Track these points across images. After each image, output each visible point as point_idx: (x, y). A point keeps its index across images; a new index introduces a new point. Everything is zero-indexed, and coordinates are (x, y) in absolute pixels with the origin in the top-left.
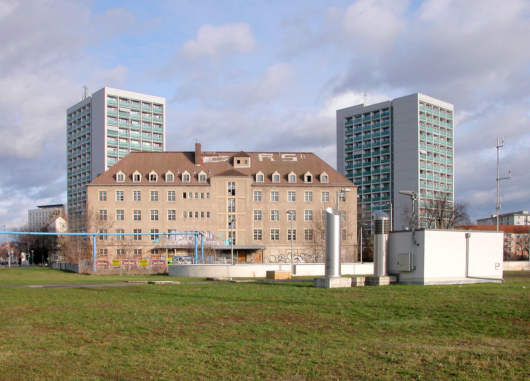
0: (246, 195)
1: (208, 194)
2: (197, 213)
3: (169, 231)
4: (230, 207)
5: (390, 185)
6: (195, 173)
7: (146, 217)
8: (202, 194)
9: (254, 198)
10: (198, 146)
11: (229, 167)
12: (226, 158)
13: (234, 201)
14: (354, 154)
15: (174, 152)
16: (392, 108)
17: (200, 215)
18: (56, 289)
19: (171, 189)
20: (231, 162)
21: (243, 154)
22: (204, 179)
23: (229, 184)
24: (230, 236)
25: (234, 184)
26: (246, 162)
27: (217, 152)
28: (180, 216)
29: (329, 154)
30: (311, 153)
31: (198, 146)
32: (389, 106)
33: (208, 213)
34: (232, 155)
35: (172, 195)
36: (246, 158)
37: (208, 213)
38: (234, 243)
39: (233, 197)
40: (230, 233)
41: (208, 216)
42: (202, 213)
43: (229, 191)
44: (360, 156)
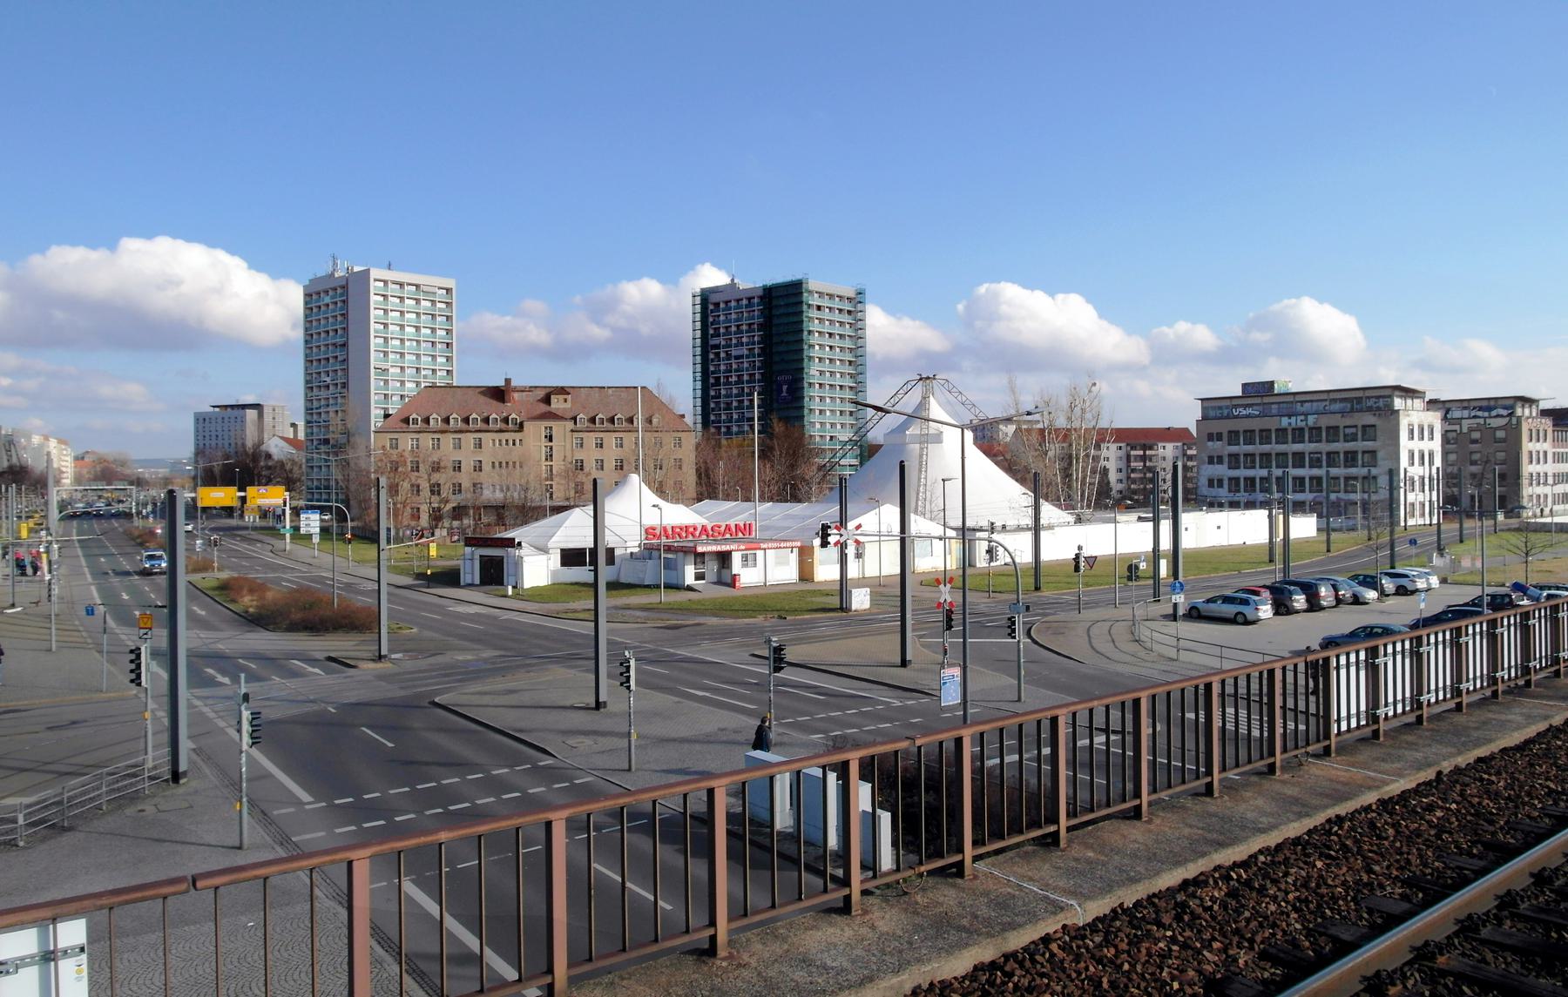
10: (508, 381)
21: (562, 391)
31: (508, 381)
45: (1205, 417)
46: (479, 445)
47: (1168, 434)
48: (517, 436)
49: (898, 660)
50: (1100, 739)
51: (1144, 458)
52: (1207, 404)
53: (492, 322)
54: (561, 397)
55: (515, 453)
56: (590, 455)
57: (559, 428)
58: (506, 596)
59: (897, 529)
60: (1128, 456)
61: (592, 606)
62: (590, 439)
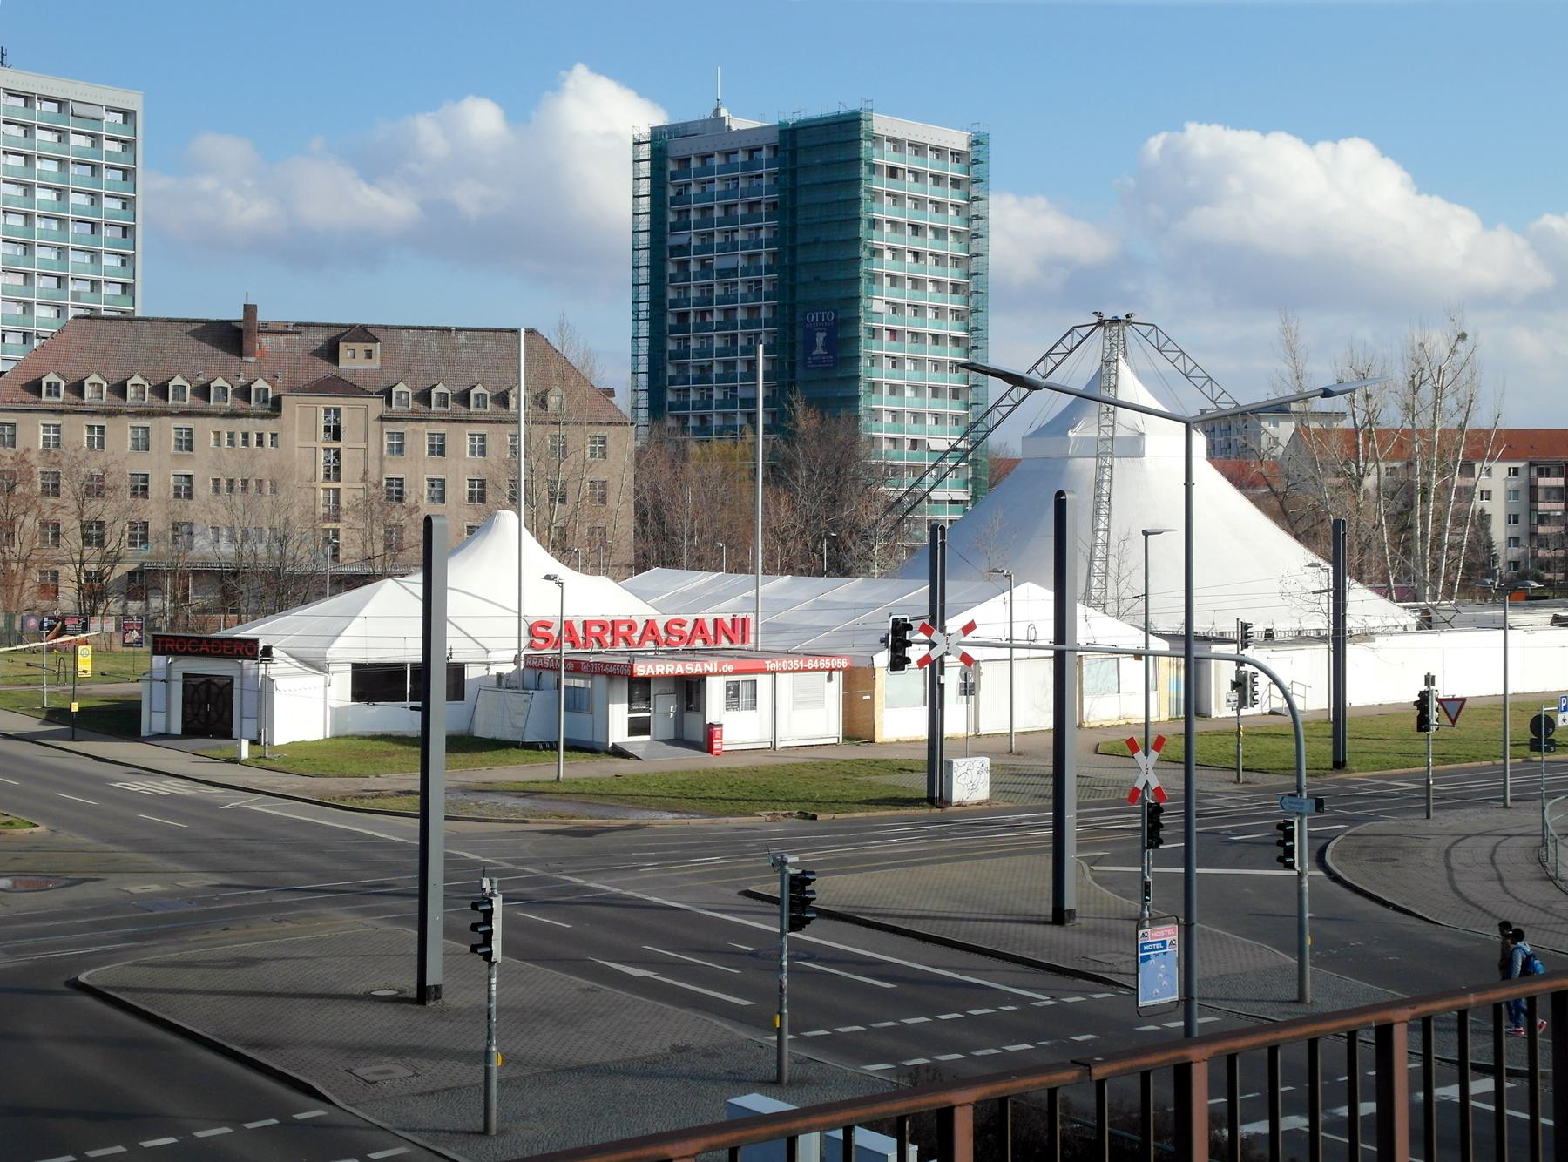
0: (366, 440)
1: (274, 435)
6: (201, 379)
8: (260, 436)
9: (130, 442)
10: (250, 310)
15: (423, 329)
18: (1374, 757)
20: (331, 352)
21: (363, 333)
22: (265, 401)
23: (327, 411)
25: (338, 411)
26: (369, 354)
27: (297, 325)
28: (202, 489)
29: (604, 336)
31: (250, 310)
34: (339, 331)
35: (477, 444)
36: (370, 346)
39: (336, 445)
41: (274, 491)
43: (327, 429)
46: (187, 442)
48: (267, 427)
49: (1047, 909)
54: (360, 348)
56: (417, 470)
57: (353, 412)
58: (235, 761)
62: (419, 436)
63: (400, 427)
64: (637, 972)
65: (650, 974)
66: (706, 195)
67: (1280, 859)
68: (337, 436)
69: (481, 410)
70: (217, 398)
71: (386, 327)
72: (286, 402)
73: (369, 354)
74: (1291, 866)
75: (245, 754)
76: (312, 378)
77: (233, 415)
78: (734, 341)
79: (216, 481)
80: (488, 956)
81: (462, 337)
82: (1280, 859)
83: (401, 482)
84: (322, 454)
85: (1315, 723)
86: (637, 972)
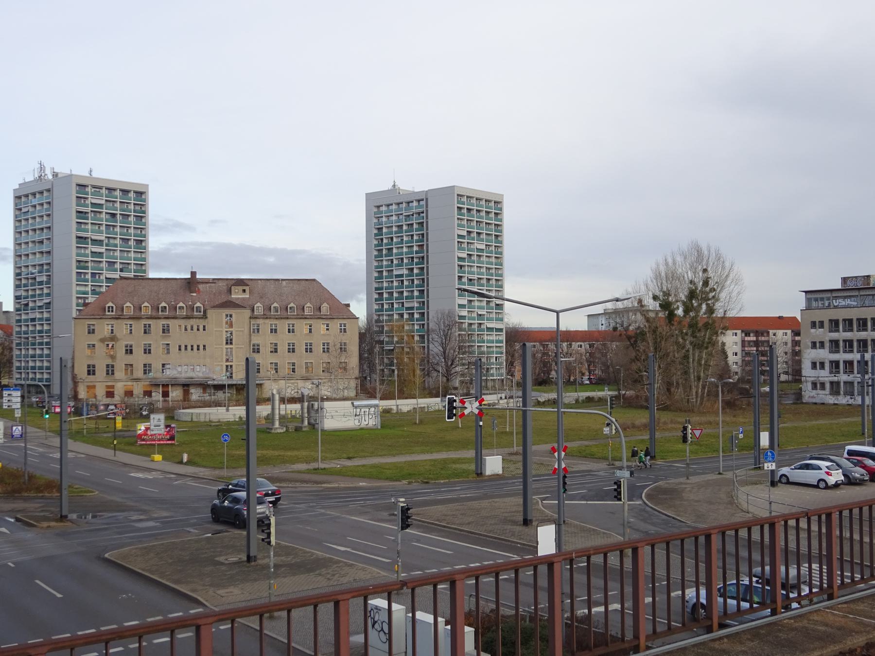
2: (192, 346)
3: (163, 365)
4: (227, 340)
5: (426, 326)
7: (138, 351)
10: (193, 274)
11: (224, 298)
12: (223, 286)
13: (231, 334)
14: (395, 273)
16: (427, 199)
17: (195, 348)
19: (165, 322)
20: (230, 291)
21: (240, 282)
23: (227, 316)
24: (227, 371)
25: (231, 316)
26: (244, 291)
30: (314, 280)
31: (193, 274)
32: (424, 197)
33: (204, 346)
36: (244, 288)
37: (204, 346)
38: (231, 377)
40: (227, 366)
42: (198, 346)
44: (402, 276)
45: (809, 308)
46: (166, 330)
47: (781, 322)
48: (201, 323)
49: (521, 519)
50: (690, 593)
51: (757, 344)
52: (809, 296)
53: (707, 430)
54: (241, 288)
55: (200, 338)
56: (264, 339)
57: (241, 317)
58: (181, 462)
59: (521, 588)
60: (743, 341)
61: (245, 473)
62: (266, 325)
63: (291, 322)
64: (343, 549)
65: (348, 549)
66: (389, 221)
67: (615, 497)
68: (231, 326)
69: (110, 313)
70: (162, 311)
71: (252, 280)
72: (211, 313)
73: (244, 291)
74: (620, 500)
75: (185, 460)
76: (220, 302)
77: (187, 317)
78: (413, 282)
79: (180, 346)
80: (269, 543)
81: (284, 283)
82: (615, 497)
83: (258, 345)
84: (224, 333)
85: (491, 446)
86: (343, 549)
